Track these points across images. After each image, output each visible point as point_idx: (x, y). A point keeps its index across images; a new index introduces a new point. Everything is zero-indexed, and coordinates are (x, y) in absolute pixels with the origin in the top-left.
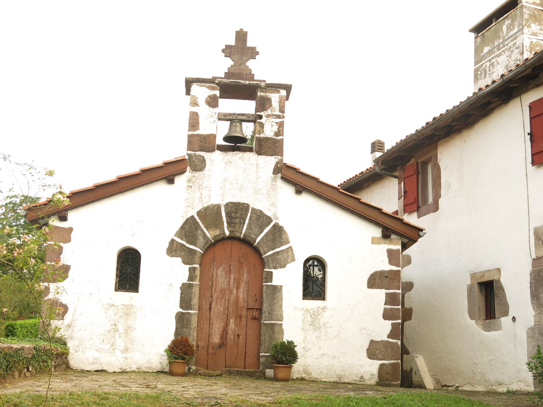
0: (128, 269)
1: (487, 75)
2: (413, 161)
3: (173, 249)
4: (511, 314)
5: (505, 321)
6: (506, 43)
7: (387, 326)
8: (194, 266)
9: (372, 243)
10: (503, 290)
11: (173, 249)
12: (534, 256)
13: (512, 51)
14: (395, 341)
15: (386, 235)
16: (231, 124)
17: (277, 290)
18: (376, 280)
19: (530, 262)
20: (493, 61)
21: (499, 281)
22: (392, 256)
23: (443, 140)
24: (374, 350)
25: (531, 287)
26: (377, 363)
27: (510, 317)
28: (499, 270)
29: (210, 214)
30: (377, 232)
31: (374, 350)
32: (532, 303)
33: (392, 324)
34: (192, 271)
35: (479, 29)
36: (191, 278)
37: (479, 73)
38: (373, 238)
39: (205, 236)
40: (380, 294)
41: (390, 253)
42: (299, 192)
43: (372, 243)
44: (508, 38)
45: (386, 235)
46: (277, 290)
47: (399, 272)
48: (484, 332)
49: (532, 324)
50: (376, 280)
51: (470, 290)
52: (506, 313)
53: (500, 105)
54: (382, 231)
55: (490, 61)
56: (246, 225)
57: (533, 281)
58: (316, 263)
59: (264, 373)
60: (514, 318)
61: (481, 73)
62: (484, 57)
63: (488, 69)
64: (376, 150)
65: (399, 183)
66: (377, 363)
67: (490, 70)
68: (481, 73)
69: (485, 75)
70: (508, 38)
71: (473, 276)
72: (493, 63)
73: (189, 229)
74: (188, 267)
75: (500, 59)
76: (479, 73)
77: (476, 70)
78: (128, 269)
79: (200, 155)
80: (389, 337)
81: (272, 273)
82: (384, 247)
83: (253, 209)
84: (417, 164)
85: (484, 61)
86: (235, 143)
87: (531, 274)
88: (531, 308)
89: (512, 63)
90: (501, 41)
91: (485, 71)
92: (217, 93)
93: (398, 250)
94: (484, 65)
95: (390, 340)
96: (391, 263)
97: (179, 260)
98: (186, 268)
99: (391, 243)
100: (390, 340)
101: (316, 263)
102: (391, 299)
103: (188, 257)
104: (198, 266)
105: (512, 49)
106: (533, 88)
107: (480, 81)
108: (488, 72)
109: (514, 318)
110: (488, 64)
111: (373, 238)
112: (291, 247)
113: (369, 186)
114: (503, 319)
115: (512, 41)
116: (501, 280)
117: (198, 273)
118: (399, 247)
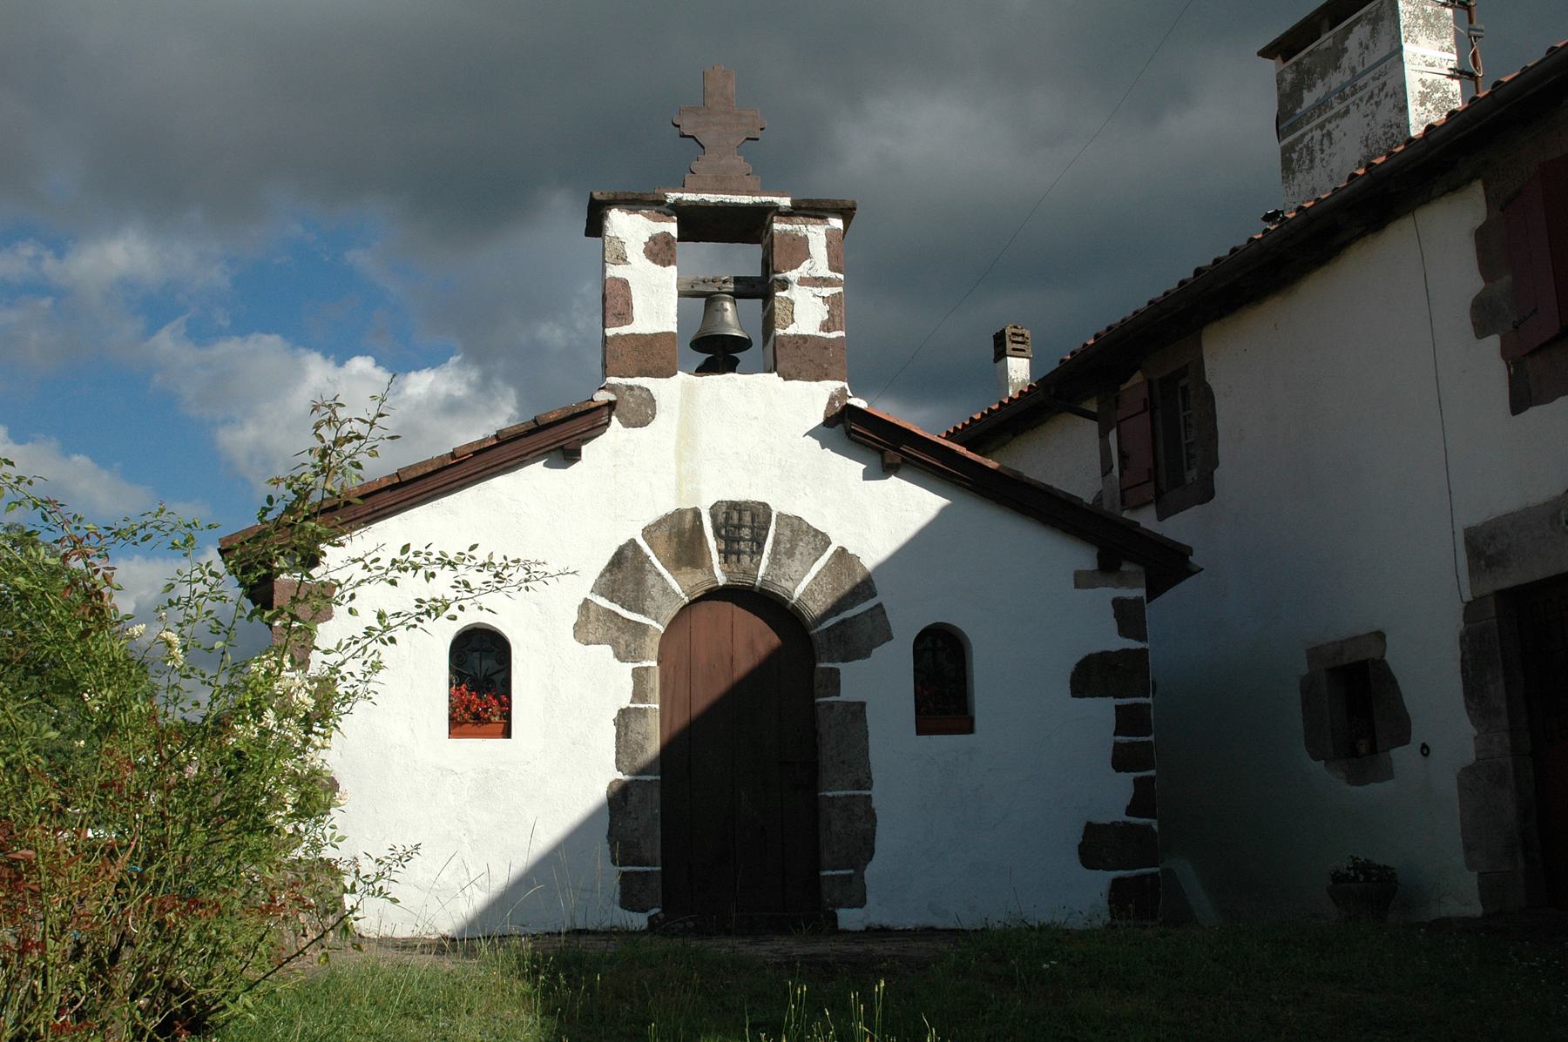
0: (481, 677)
1: (1317, 161)
2: (1138, 378)
3: (589, 625)
4: (1417, 736)
5: (1404, 757)
6: (1360, 83)
7: (1122, 786)
8: (645, 664)
9: (1077, 586)
10: (1394, 682)
11: (589, 625)
12: (1468, 597)
13: (1377, 104)
14: (1146, 820)
15: (1108, 566)
16: (707, 305)
17: (857, 711)
18: (1091, 676)
19: (1458, 609)
20: (1329, 127)
21: (1381, 664)
22: (1129, 617)
23: (1216, 325)
24: (1097, 846)
25: (1463, 671)
26: (1104, 878)
27: (1413, 748)
28: (1380, 636)
29: (680, 534)
30: (1084, 557)
31: (1097, 846)
32: (1468, 708)
33: (1136, 781)
34: (639, 675)
35: (1282, 49)
36: (639, 693)
37: (1295, 156)
38: (1077, 574)
39: (666, 590)
40: (1103, 709)
41: (1120, 606)
42: (567, 455)
43: (1077, 586)
44: (1364, 73)
45: (1108, 566)
46: (857, 711)
47: (1144, 651)
48: (1348, 787)
49: (1471, 758)
50: (1091, 676)
51: (1308, 688)
52: (1403, 738)
53: (1362, 235)
54: (1100, 556)
55: (1321, 126)
56: (765, 555)
57: (1467, 656)
58: (940, 643)
59: (835, 919)
60: (1424, 746)
61: (1300, 157)
62: (1307, 118)
63: (1317, 147)
64: (1008, 351)
65: (1103, 435)
66: (1104, 878)
67: (1322, 151)
68: (1300, 157)
69: (1312, 161)
70: (1364, 73)
71: (1314, 654)
72: (1329, 134)
73: (624, 570)
74: (629, 667)
75: (1344, 123)
76: (1295, 156)
77: (1286, 152)
78: (481, 677)
79: (640, 387)
80: (1130, 811)
81: (837, 671)
82: (1105, 595)
83: (780, 516)
84: (1150, 383)
85: (1307, 128)
86: (718, 354)
87: (1462, 640)
88: (1466, 721)
89: (1380, 132)
90: (1348, 77)
91: (1311, 151)
92: (672, 228)
93: (1139, 601)
94: (1308, 138)
95: (1133, 820)
96: (1123, 632)
97: (607, 650)
98: (624, 673)
99: (1121, 583)
100: (1133, 820)
101: (940, 643)
102: (1128, 720)
103: (626, 641)
104: (654, 664)
105: (1376, 99)
106: (1443, 194)
107: (1299, 176)
108: (1318, 155)
109: (1424, 746)
110: (1317, 134)
111: (1077, 574)
112: (880, 606)
113: (1004, 444)
114: (1397, 753)
115: (1374, 79)
116: (1387, 658)
117: (655, 682)
118: (1141, 592)
